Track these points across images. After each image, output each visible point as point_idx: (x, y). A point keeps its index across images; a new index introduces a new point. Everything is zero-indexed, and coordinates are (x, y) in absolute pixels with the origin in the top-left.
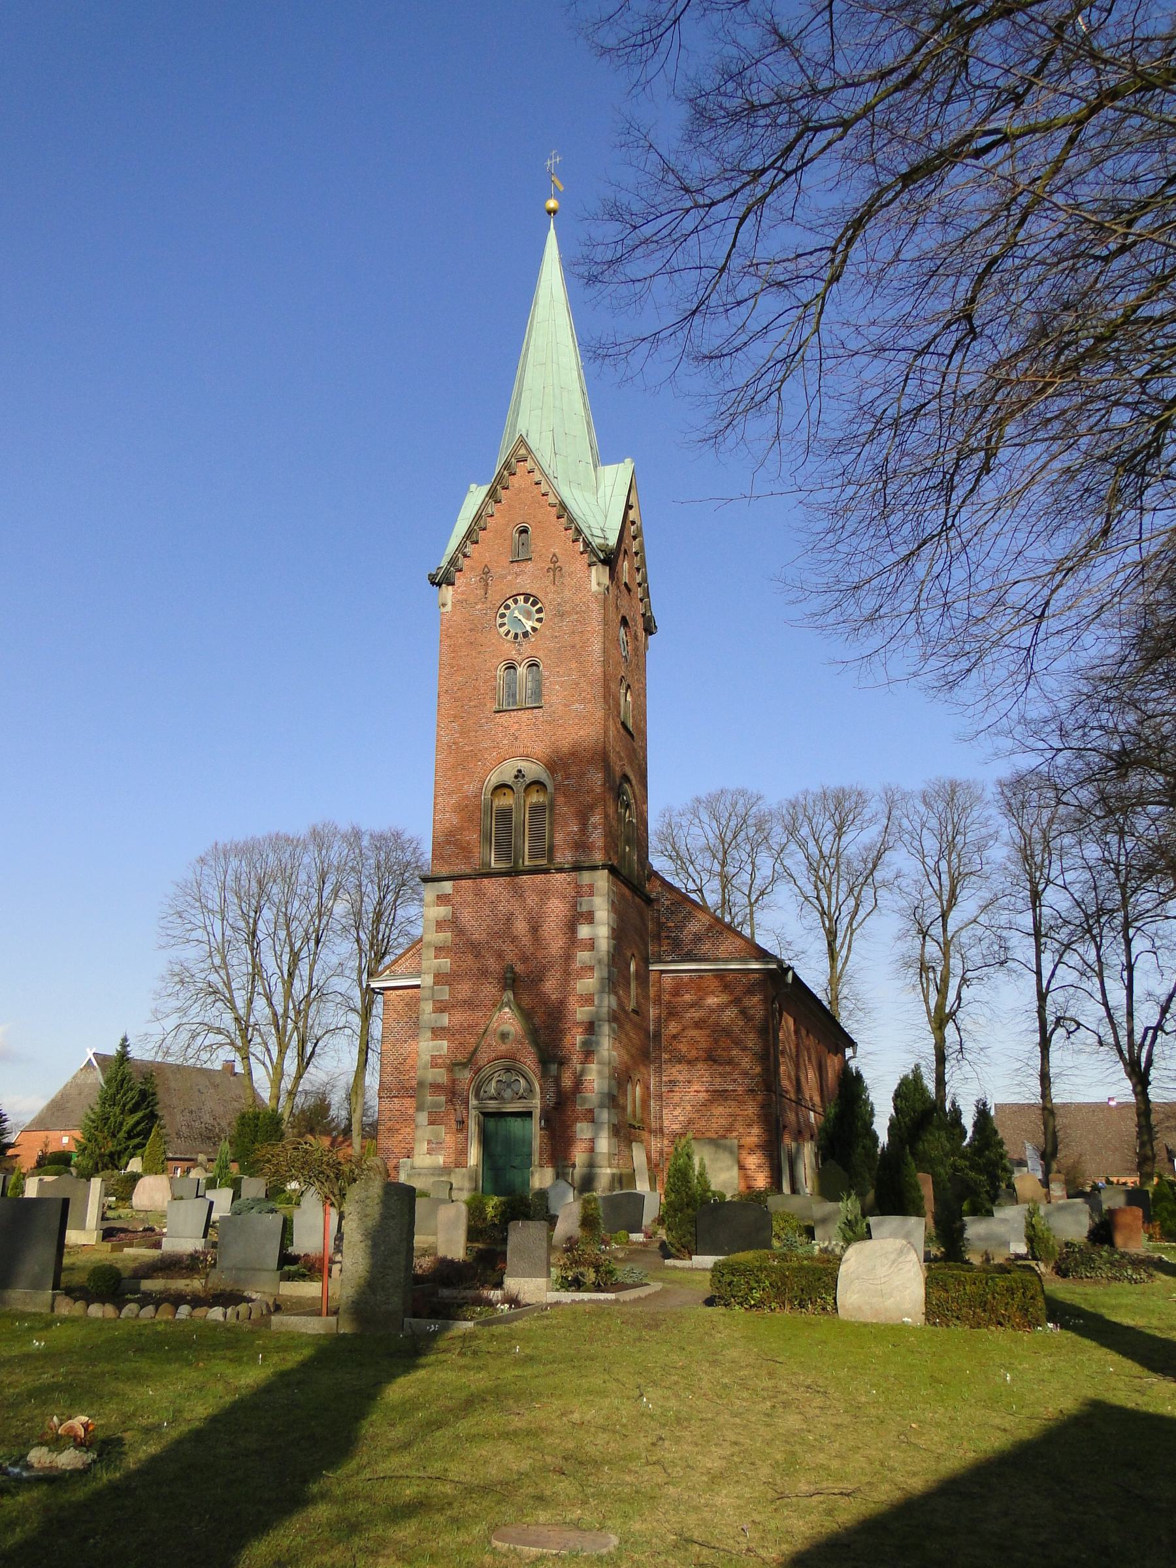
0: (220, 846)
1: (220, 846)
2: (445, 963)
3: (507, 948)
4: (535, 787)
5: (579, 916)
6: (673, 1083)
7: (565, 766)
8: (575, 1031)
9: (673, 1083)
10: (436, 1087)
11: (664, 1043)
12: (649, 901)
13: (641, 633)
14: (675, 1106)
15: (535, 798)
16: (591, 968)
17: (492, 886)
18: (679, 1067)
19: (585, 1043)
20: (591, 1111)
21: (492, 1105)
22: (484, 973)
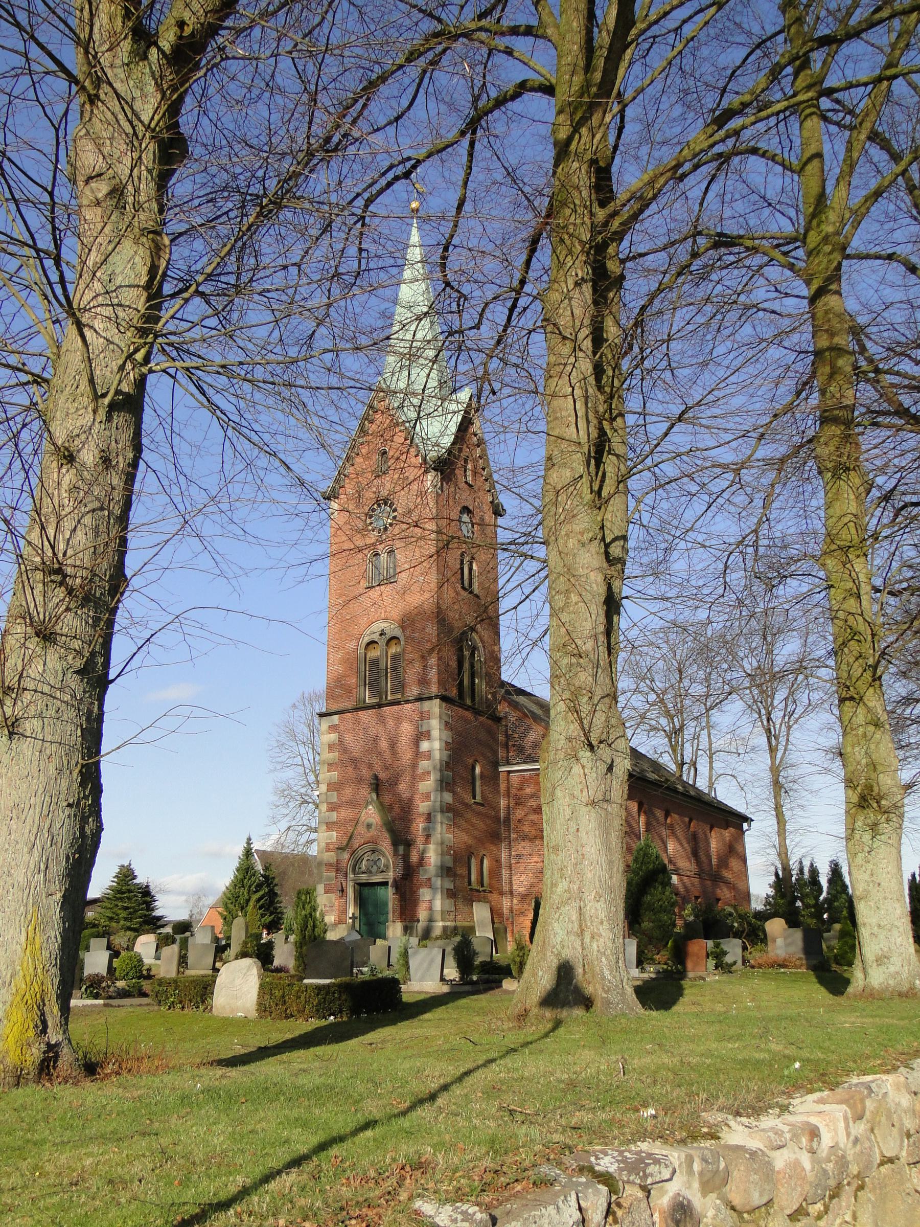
0: (306, 695)
1: (306, 695)
2: (334, 775)
3: (375, 760)
4: (394, 642)
5: (421, 735)
6: (519, 856)
7: (413, 622)
8: (418, 820)
9: (519, 856)
10: (329, 865)
11: (512, 826)
12: (498, 720)
13: (489, 517)
14: (521, 874)
15: (394, 649)
16: (429, 773)
17: (366, 716)
18: (523, 844)
19: (425, 829)
20: (429, 879)
21: (364, 878)
22: (360, 780)
